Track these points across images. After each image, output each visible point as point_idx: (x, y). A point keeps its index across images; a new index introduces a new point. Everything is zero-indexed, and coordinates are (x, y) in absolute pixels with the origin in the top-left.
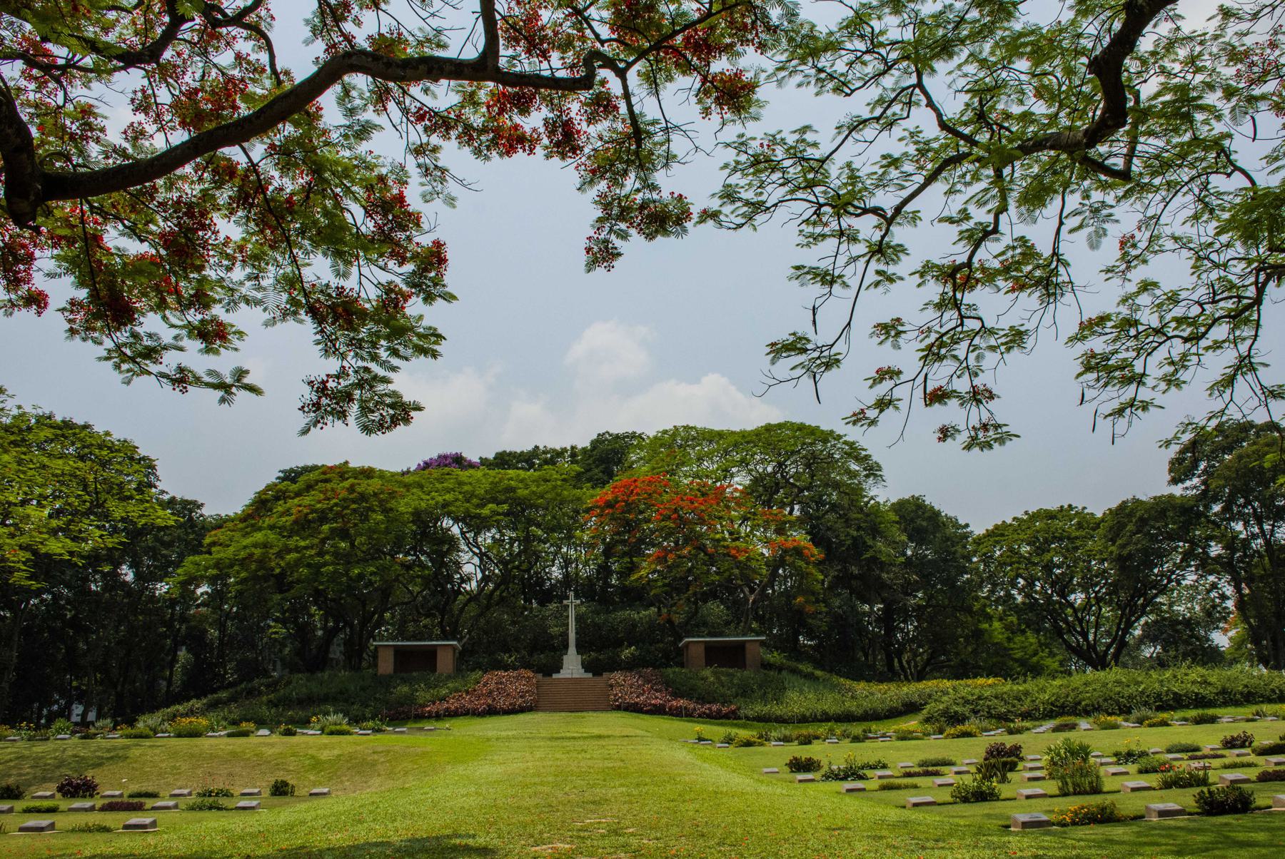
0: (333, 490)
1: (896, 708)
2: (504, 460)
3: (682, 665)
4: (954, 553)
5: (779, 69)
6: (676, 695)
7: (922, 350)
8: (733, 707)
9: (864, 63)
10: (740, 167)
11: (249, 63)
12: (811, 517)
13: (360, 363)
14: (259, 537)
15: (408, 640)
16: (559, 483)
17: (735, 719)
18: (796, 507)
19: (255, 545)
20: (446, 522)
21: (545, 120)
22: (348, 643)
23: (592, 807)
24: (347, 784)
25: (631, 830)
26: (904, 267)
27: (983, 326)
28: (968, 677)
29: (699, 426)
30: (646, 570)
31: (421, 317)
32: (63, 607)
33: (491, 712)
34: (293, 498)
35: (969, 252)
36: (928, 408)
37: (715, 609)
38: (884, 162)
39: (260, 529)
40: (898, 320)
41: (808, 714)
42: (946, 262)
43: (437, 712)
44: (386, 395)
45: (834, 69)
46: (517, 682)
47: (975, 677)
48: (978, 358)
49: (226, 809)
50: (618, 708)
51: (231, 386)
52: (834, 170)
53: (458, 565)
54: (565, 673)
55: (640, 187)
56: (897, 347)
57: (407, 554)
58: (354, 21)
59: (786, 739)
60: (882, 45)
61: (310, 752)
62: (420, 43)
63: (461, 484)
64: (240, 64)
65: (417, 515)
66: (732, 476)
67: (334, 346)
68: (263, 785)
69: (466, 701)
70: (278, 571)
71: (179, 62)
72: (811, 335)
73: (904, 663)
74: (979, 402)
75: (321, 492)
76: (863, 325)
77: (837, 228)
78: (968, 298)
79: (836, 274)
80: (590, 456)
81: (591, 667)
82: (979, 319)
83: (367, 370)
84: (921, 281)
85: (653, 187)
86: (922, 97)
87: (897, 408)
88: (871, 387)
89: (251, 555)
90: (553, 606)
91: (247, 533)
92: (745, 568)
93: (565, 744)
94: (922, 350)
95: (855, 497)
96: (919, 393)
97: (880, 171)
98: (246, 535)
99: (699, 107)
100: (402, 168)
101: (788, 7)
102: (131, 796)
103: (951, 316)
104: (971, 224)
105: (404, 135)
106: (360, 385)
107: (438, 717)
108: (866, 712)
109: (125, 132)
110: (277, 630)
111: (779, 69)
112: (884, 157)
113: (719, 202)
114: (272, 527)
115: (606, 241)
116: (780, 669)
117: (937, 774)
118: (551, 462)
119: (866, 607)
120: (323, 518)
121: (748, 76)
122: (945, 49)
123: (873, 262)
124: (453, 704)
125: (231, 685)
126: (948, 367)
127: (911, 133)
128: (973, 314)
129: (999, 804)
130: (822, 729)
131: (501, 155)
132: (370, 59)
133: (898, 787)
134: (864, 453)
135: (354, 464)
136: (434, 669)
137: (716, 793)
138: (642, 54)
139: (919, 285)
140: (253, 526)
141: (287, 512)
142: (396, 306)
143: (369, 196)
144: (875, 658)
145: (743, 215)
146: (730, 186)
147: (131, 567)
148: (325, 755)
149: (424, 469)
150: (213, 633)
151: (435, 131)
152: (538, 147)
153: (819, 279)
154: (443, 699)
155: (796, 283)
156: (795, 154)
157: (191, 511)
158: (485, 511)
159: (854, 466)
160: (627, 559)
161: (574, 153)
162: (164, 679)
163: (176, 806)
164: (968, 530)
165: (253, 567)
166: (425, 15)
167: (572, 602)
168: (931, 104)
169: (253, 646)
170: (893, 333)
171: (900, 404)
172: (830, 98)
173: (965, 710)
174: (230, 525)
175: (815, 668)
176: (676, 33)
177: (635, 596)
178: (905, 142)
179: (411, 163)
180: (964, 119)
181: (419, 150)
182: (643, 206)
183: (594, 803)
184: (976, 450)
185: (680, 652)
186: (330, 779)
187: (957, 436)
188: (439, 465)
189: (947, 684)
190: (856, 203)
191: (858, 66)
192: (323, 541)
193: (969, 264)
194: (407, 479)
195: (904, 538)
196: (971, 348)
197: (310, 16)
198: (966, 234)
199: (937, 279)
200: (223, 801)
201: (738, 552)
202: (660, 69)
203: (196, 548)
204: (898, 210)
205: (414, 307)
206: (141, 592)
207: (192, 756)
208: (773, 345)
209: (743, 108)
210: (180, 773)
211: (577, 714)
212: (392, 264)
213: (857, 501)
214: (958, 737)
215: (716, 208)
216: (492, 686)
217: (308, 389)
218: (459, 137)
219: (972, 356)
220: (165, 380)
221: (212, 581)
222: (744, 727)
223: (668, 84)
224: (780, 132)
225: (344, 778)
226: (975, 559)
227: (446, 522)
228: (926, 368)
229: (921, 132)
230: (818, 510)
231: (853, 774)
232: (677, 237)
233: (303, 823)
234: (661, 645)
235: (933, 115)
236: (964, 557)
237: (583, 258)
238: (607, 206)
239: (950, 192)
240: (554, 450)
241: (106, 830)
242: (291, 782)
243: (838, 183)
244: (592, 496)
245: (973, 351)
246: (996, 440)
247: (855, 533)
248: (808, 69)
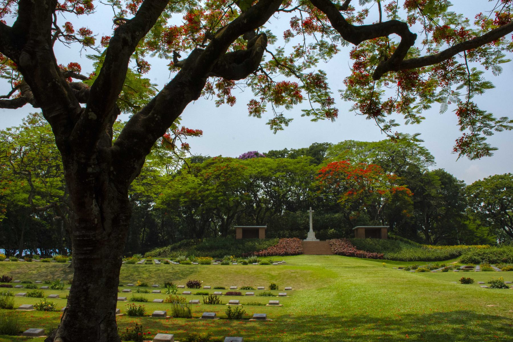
2: (273, 154)
6: (359, 249)
8: (382, 254)
33: (286, 254)
41: (412, 258)
46: (293, 243)
50: (336, 254)
63: (267, 164)
108: (436, 257)
116: (396, 239)
124: (270, 250)
135: (224, 156)
136: (258, 237)
164: (464, 183)
165: (190, 197)
188: (249, 157)
214: (509, 270)
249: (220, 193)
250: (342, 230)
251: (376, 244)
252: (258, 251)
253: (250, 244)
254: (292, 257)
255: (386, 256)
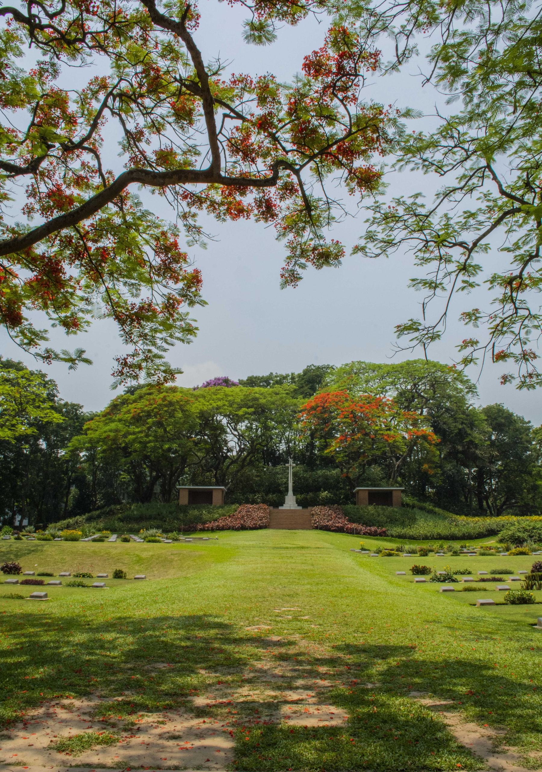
0: (154, 399)
1: (482, 532)
2: (252, 382)
3: (354, 503)
4: (521, 439)
5: (399, 161)
6: (351, 521)
7: (492, 328)
8: (384, 529)
9: (454, 153)
10: (376, 221)
11: (89, 167)
12: (433, 416)
13: (146, 347)
14: (113, 426)
15: (197, 485)
16: (284, 395)
17: (385, 536)
18: (425, 410)
19: (111, 431)
20: (219, 418)
21: (255, 199)
22: (163, 486)
23: (288, 598)
24: (156, 572)
25: (306, 617)
26: (479, 278)
27: (530, 314)
28: (527, 515)
29: (367, 361)
30: (335, 446)
31: (188, 314)
32: (9, 462)
33: (243, 528)
34: (132, 404)
35: (520, 269)
36: (495, 363)
37: (376, 470)
38: (465, 215)
39: (114, 421)
40: (477, 310)
41: (429, 535)
42: (508, 275)
43: (212, 528)
44: (161, 365)
45: (434, 159)
47: (531, 515)
48: (527, 333)
49: (87, 586)
50: (317, 528)
51: (75, 360)
52: (436, 221)
53: (226, 442)
54: (286, 507)
55: (313, 237)
56: (476, 326)
57: (197, 435)
58: (146, 142)
59: (413, 552)
60: (464, 142)
61: (136, 553)
62: (185, 153)
63: (227, 395)
64: (84, 168)
65: (203, 415)
66: (386, 391)
67: (131, 337)
68: (110, 572)
69: (229, 522)
70: (123, 445)
71: (51, 168)
72: (421, 321)
73: (490, 504)
74: (527, 360)
75: (147, 400)
76: (454, 314)
77: (438, 255)
78: (520, 296)
79: (438, 282)
80: (303, 379)
81: (302, 503)
82: (528, 309)
83: (150, 351)
84: (491, 286)
85: (320, 237)
86: (490, 173)
87: (476, 364)
88: (459, 351)
89: (109, 436)
90: (279, 467)
91: (107, 423)
92: (394, 447)
93: (281, 552)
94: (492, 328)
95: (460, 404)
96: (489, 354)
97: (464, 221)
98: (106, 424)
99: (347, 188)
100: (176, 227)
101: (399, 127)
102: (39, 575)
103: (509, 306)
104: (522, 251)
105: (176, 207)
106: (146, 359)
107: (213, 530)
108: (464, 534)
109: (23, 209)
110: (125, 477)
111: (399, 161)
112: (465, 212)
113: (365, 241)
114: (120, 420)
115: (292, 271)
116: (413, 507)
117: (500, 580)
118: (279, 382)
119: (467, 471)
120: (149, 415)
121: (376, 169)
122: (502, 146)
123: (460, 275)
124: (221, 523)
125: (99, 508)
126: (508, 338)
127: (485, 195)
128: (524, 306)
129: (532, 606)
130: (436, 545)
131: (233, 219)
132: (144, 174)
133: (474, 590)
134: (466, 378)
136: (211, 503)
137: (362, 591)
138: (311, 158)
139: (490, 289)
140: (110, 419)
141: (128, 412)
142: (173, 307)
143: (157, 244)
144: (471, 501)
145: (381, 248)
146: (371, 232)
147: (44, 440)
148: (144, 555)
149: (206, 387)
150: (90, 478)
151: (194, 204)
152: (252, 214)
153: (427, 285)
154: (216, 520)
155: (412, 289)
156: (411, 210)
157: (76, 410)
158: (240, 413)
159: (460, 386)
160: (323, 440)
161: (273, 218)
162: (63, 502)
163: (60, 584)
164: (530, 425)
165: (110, 443)
166: (184, 138)
167: (291, 463)
168: (495, 178)
169: (111, 486)
170: (473, 318)
171: (477, 361)
172: (433, 175)
173: (525, 535)
174: (97, 418)
175: (435, 506)
176: (331, 146)
177: (329, 462)
178: (481, 200)
179: (180, 224)
180: (518, 185)
181: (185, 216)
182: (315, 249)
183: (289, 596)
184: (525, 389)
185: (354, 495)
186: (147, 569)
187: (513, 380)
188: (215, 385)
189: (514, 518)
190: (449, 240)
191: (450, 155)
192: (149, 429)
193: (520, 276)
194: (196, 393)
195: (491, 430)
196: (523, 327)
197: (121, 140)
198: (519, 258)
199: (501, 285)
200: (86, 581)
201: (388, 437)
202: (324, 166)
203: (78, 430)
204: (475, 244)
205: (183, 308)
206: (50, 455)
207: (72, 552)
208: (398, 327)
209: (374, 188)
210: (65, 563)
211: (292, 531)
212: (171, 283)
213: (462, 407)
214: (517, 554)
215: (363, 245)
216: (244, 513)
217: (117, 363)
218: (208, 208)
219: (523, 332)
220: (39, 358)
221: (87, 450)
222: (390, 541)
223: (329, 174)
224: (403, 197)
225: (155, 569)
226: (534, 443)
227: (219, 418)
228: (494, 339)
229: (491, 194)
230: (438, 412)
231: (449, 578)
232: (336, 267)
233: (125, 600)
234: (343, 491)
235: (496, 185)
236: (527, 441)
237: (280, 280)
238: (293, 249)
239: (509, 231)
240: (281, 375)
241: (21, 598)
242: (124, 570)
243: (438, 227)
244: (303, 403)
245: (524, 328)
246: (537, 383)
247: (460, 427)
248: (417, 160)
249: (150, 438)
250: (340, 494)
251: (379, 516)
252: (204, 523)
253: (196, 512)
254: (236, 533)
255: (389, 533)
